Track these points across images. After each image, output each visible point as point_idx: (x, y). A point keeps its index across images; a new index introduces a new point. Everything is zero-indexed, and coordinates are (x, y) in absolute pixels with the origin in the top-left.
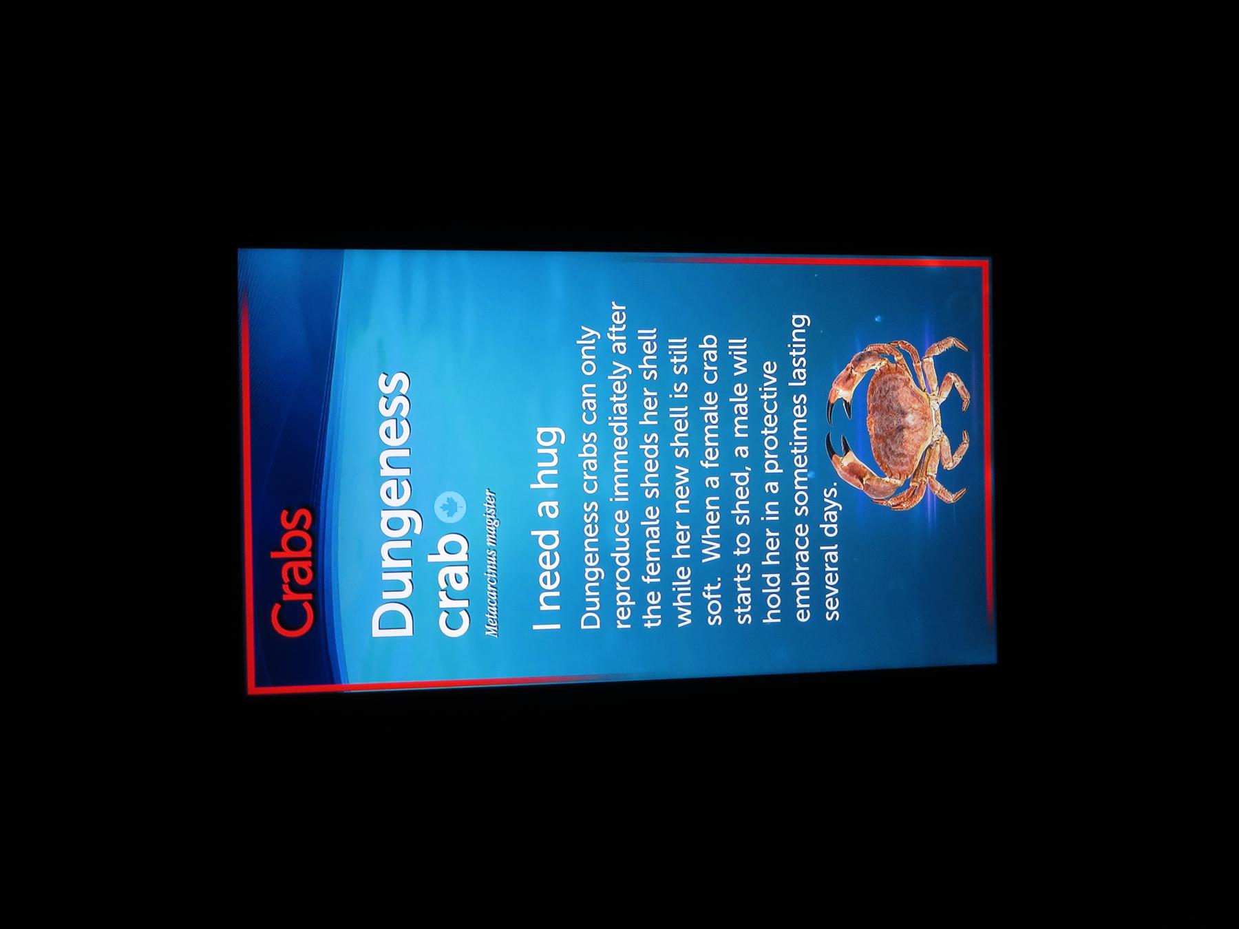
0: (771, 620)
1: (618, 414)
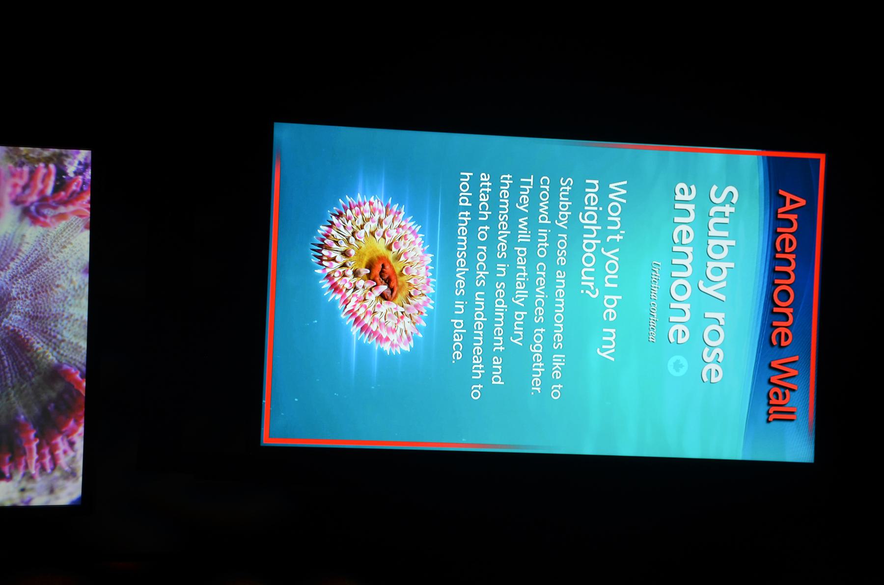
0: (468, 174)
1: (522, 282)
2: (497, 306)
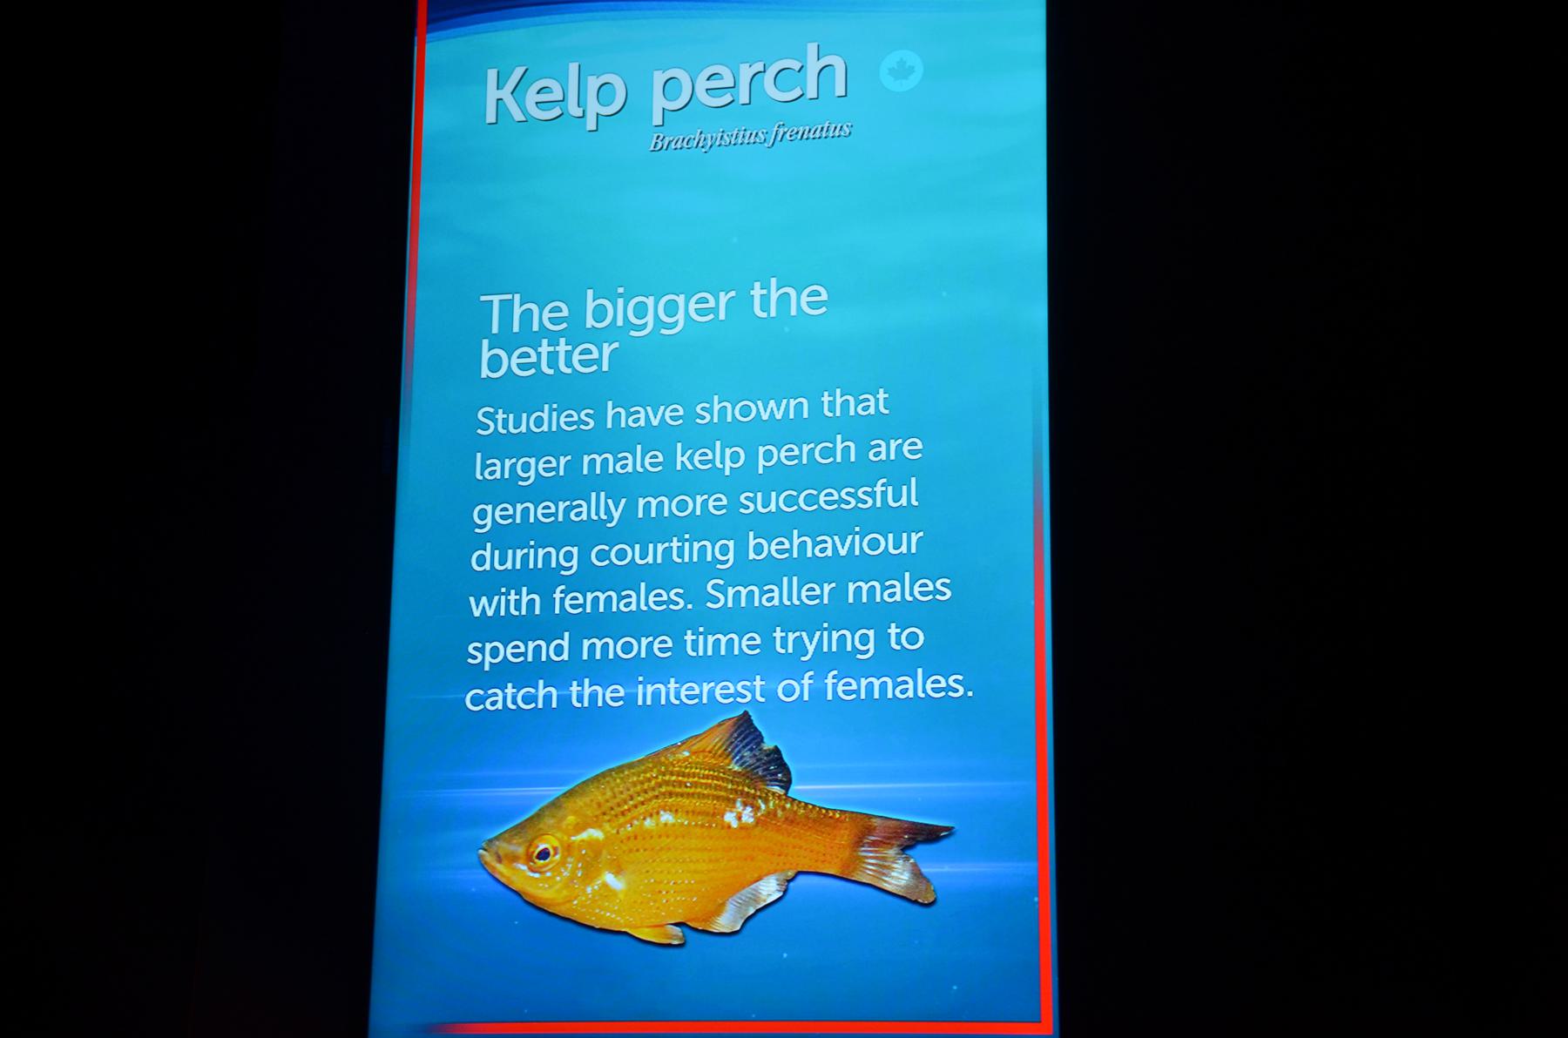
0: (610, 413)
2: (545, 428)
